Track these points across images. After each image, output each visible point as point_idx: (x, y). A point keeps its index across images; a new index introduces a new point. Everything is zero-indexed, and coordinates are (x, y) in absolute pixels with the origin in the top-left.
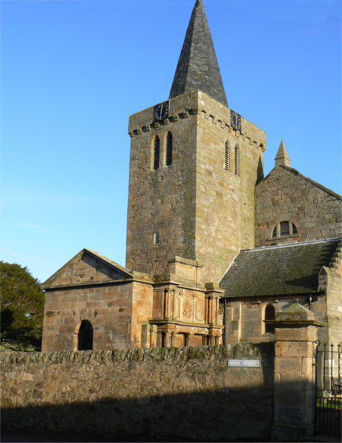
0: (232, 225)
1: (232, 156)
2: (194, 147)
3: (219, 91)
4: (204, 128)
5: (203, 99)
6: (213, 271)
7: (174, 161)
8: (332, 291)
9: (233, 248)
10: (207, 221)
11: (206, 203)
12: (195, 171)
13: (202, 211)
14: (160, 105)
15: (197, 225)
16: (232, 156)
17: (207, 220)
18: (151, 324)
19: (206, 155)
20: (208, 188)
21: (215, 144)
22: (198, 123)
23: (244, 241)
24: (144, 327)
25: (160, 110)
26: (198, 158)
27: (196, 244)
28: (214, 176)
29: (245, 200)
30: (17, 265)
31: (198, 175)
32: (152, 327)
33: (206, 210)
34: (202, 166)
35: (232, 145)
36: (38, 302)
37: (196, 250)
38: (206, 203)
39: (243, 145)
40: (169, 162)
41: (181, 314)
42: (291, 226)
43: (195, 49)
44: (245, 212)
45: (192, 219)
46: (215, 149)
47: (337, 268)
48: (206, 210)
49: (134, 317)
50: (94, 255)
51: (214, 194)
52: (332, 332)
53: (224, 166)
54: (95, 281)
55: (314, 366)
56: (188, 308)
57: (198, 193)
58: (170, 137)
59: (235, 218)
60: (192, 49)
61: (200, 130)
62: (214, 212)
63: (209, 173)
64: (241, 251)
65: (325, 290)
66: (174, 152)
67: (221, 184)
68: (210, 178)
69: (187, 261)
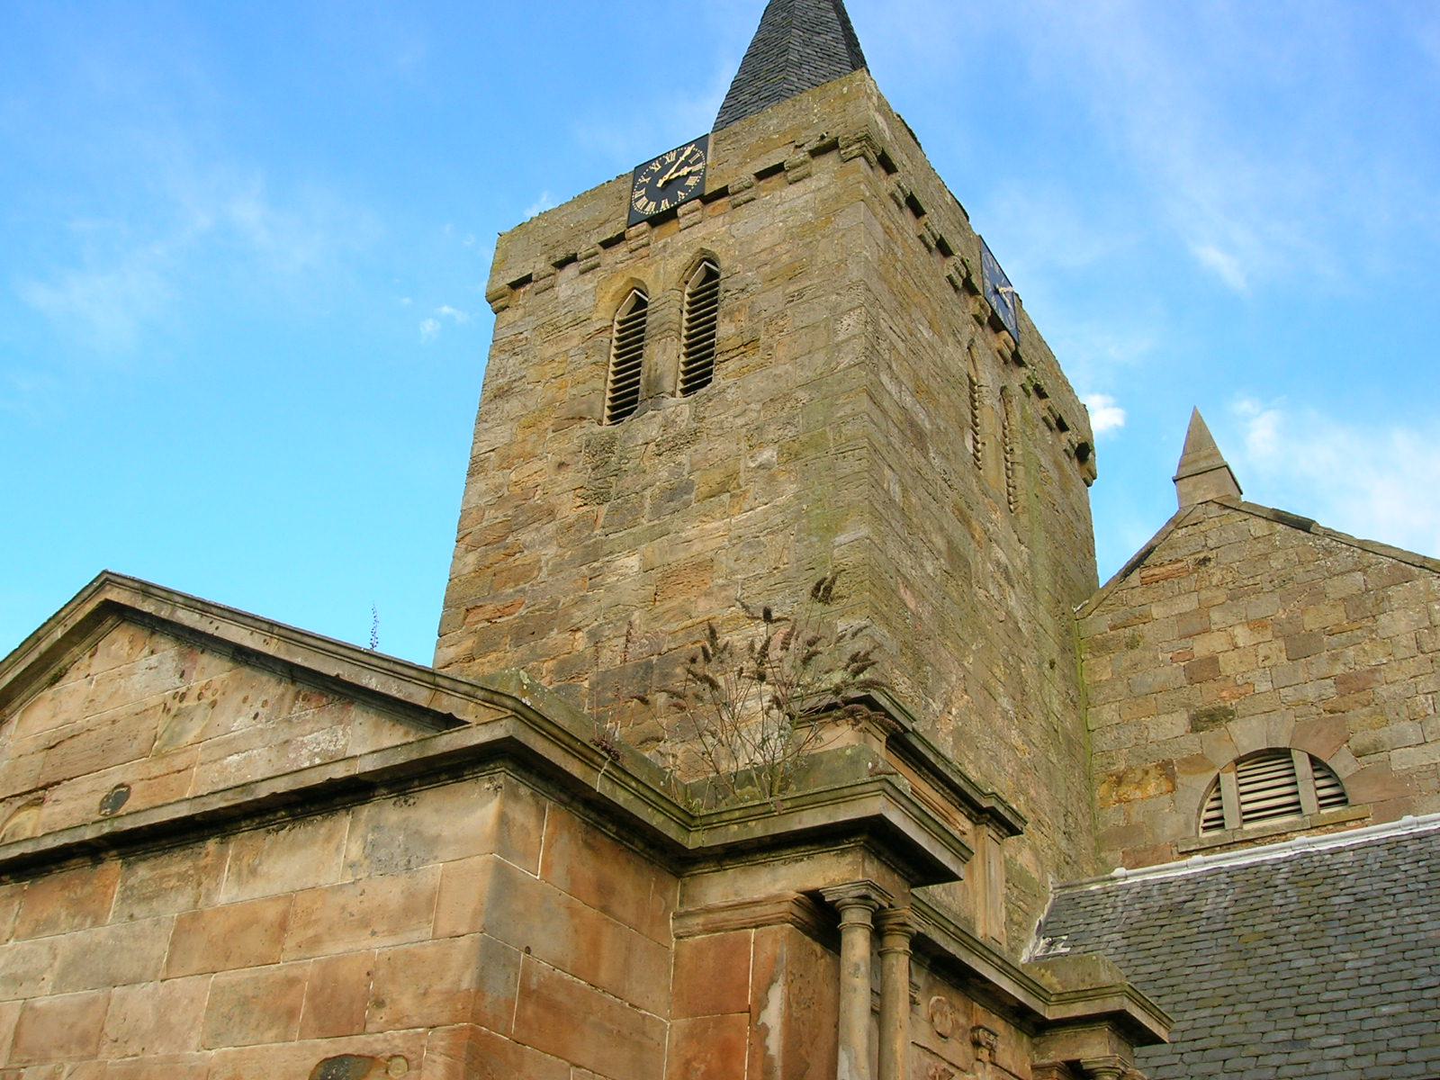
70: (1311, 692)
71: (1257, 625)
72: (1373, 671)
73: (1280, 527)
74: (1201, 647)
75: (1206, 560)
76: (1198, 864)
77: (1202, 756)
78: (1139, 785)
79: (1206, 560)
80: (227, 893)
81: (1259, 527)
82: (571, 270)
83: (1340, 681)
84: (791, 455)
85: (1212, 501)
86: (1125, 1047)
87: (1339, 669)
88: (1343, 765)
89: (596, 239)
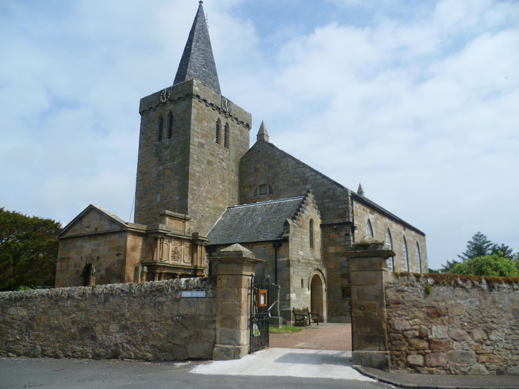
0: (221, 187)
1: (223, 133)
2: (190, 124)
3: (214, 81)
4: (198, 109)
5: (198, 86)
6: (203, 224)
7: (174, 135)
8: (294, 239)
9: (221, 205)
10: (198, 184)
11: (197, 169)
12: (189, 144)
13: (194, 175)
14: (164, 90)
15: (190, 186)
16: (223, 133)
17: (199, 183)
18: (143, 266)
19: (199, 131)
20: (200, 157)
21: (207, 122)
22: (193, 105)
23: (231, 200)
24: (136, 269)
25: (163, 95)
26: (192, 133)
27: (189, 201)
28: (206, 147)
29: (234, 168)
30: (50, 220)
31: (191, 146)
32: (143, 269)
33: (198, 174)
34: (195, 140)
35: (223, 124)
36: (53, 249)
37: (189, 206)
38: (197, 169)
39: (231, 124)
40: (170, 136)
41: (170, 258)
42: (268, 187)
43: (196, 46)
44: (233, 177)
45: (186, 181)
46: (207, 126)
47: (298, 220)
48: (198, 174)
49: (128, 259)
50: (98, 209)
51: (206, 162)
52: (294, 271)
53: (215, 140)
54: (101, 230)
55: (250, 296)
56: (176, 254)
57: (191, 161)
58: (171, 116)
59: (223, 182)
60: (193, 46)
61: (194, 111)
62: (205, 176)
63: (202, 145)
64: (228, 208)
65: (288, 237)
66: (173, 128)
67: (212, 155)
68: (202, 149)
69: (351, 210)
70: (270, 175)
71: (265, 163)
72: (279, 172)
73: (270, 146)
74: (257, 166)
75: (259, 151)
76: (246, 205)
77: (255, 185)
78: (247, 189)
79: (259, 151)
80: (108, 239)
81: (267, 146)
82: (152, 110)
83: (275, 174)
84: (181, 154)
85: (19, 355)
86: (188, 254)
87: (275, 172)
88: (273, 188)
89: (155, 105)
